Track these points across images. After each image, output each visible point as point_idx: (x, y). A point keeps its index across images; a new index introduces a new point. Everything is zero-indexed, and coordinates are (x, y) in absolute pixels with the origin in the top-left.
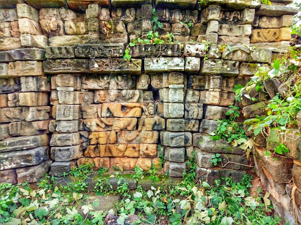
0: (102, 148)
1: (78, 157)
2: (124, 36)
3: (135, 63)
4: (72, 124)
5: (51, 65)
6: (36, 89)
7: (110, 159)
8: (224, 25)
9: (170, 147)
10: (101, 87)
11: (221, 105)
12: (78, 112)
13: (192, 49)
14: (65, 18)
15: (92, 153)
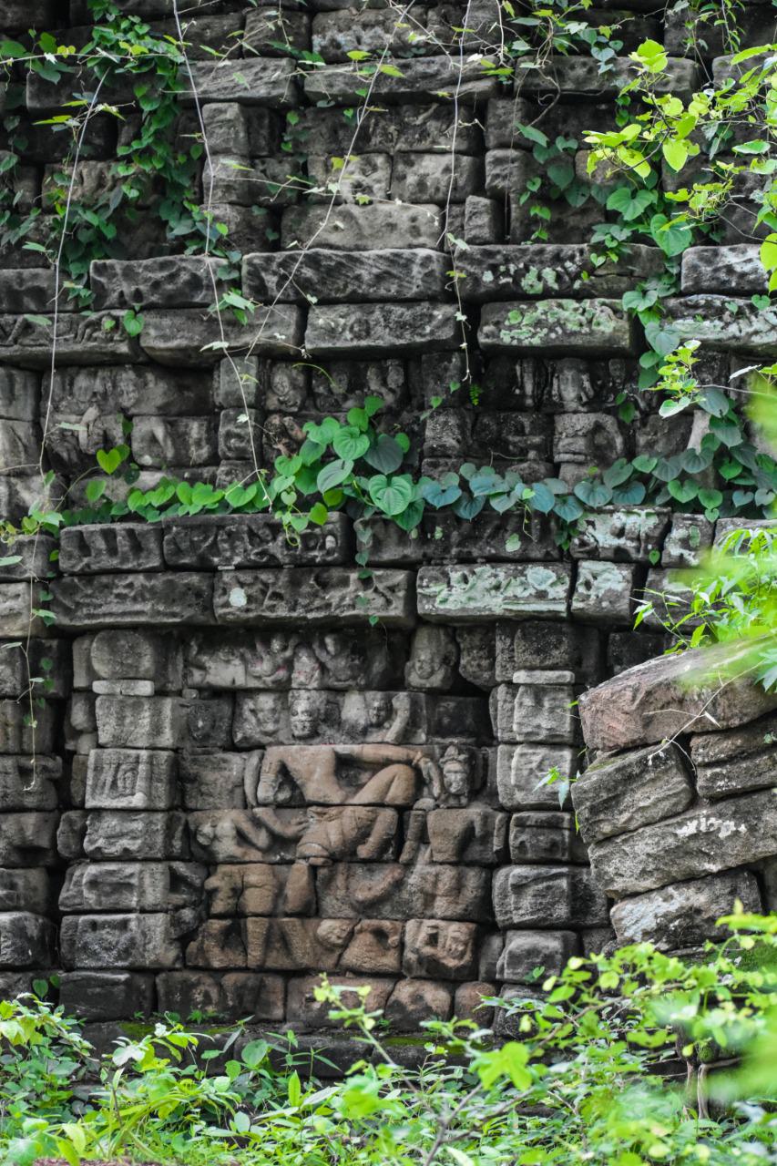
3: (381, 587)
5: (78, 598)
10: (259, 678)
15: (216, 950)
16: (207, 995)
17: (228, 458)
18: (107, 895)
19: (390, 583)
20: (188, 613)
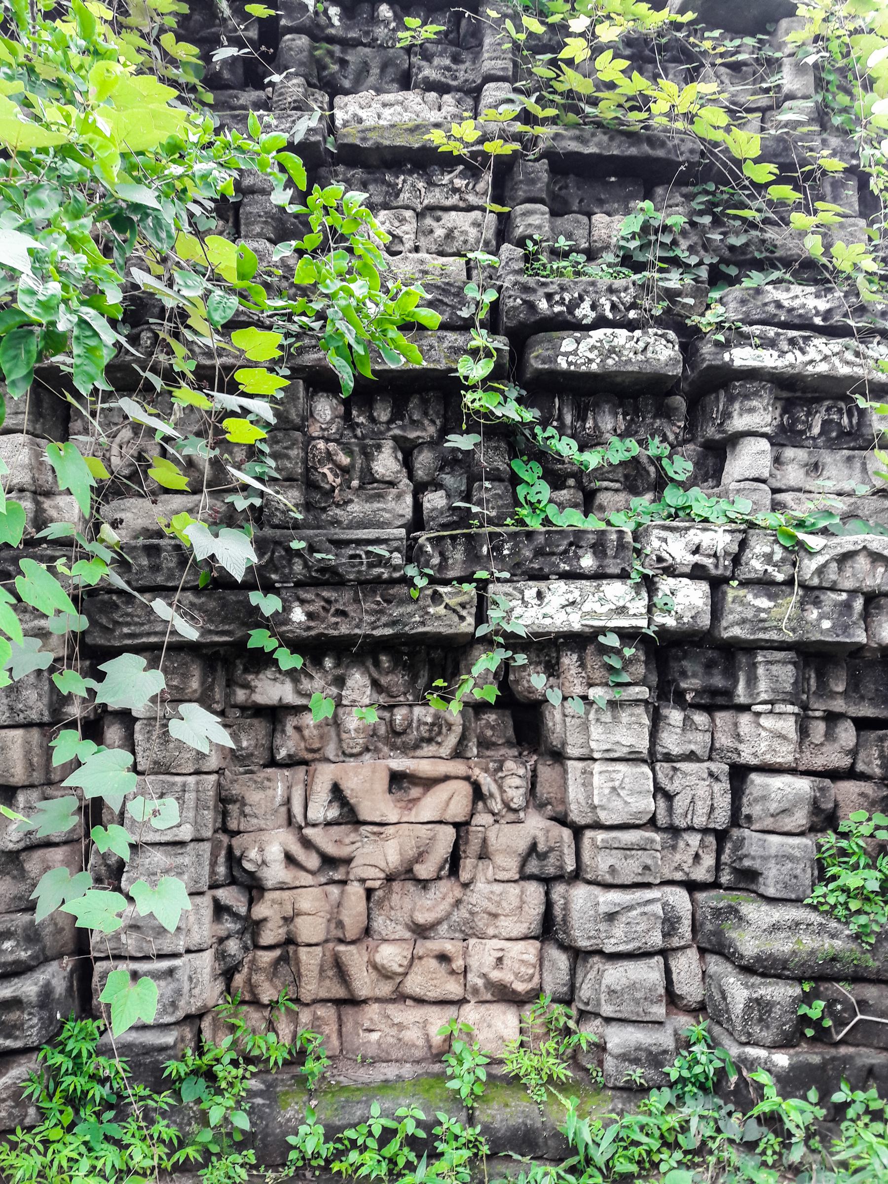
0: (310, 960)
1: (205, 1006)
2: (399, 497)
4: (187, 860)
6: (46, 713)
8: (789, 453)
9: (600, 952)
11: (802, 768)
12: (211, 804)
13: (677, 549)
15: (266, 985)
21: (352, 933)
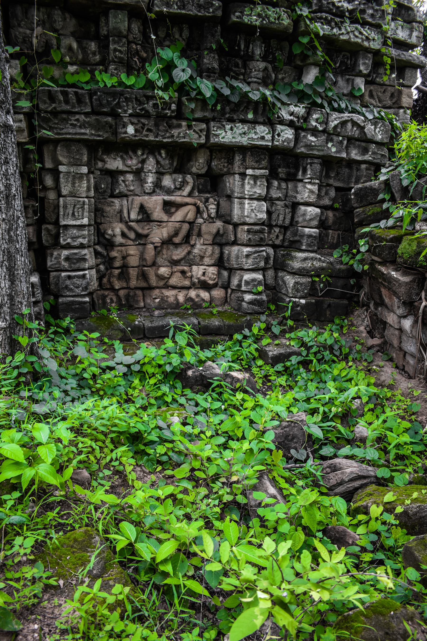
0: (133, 273)
3: (197, 129)
7: (143, 292)
14: (62, 29)
15: (116, 282)
16: (111, 299)
17: (115, 62)
18: (74, 264)
19: (200, 128)
20: (106, 135)
21: (149, 263)
